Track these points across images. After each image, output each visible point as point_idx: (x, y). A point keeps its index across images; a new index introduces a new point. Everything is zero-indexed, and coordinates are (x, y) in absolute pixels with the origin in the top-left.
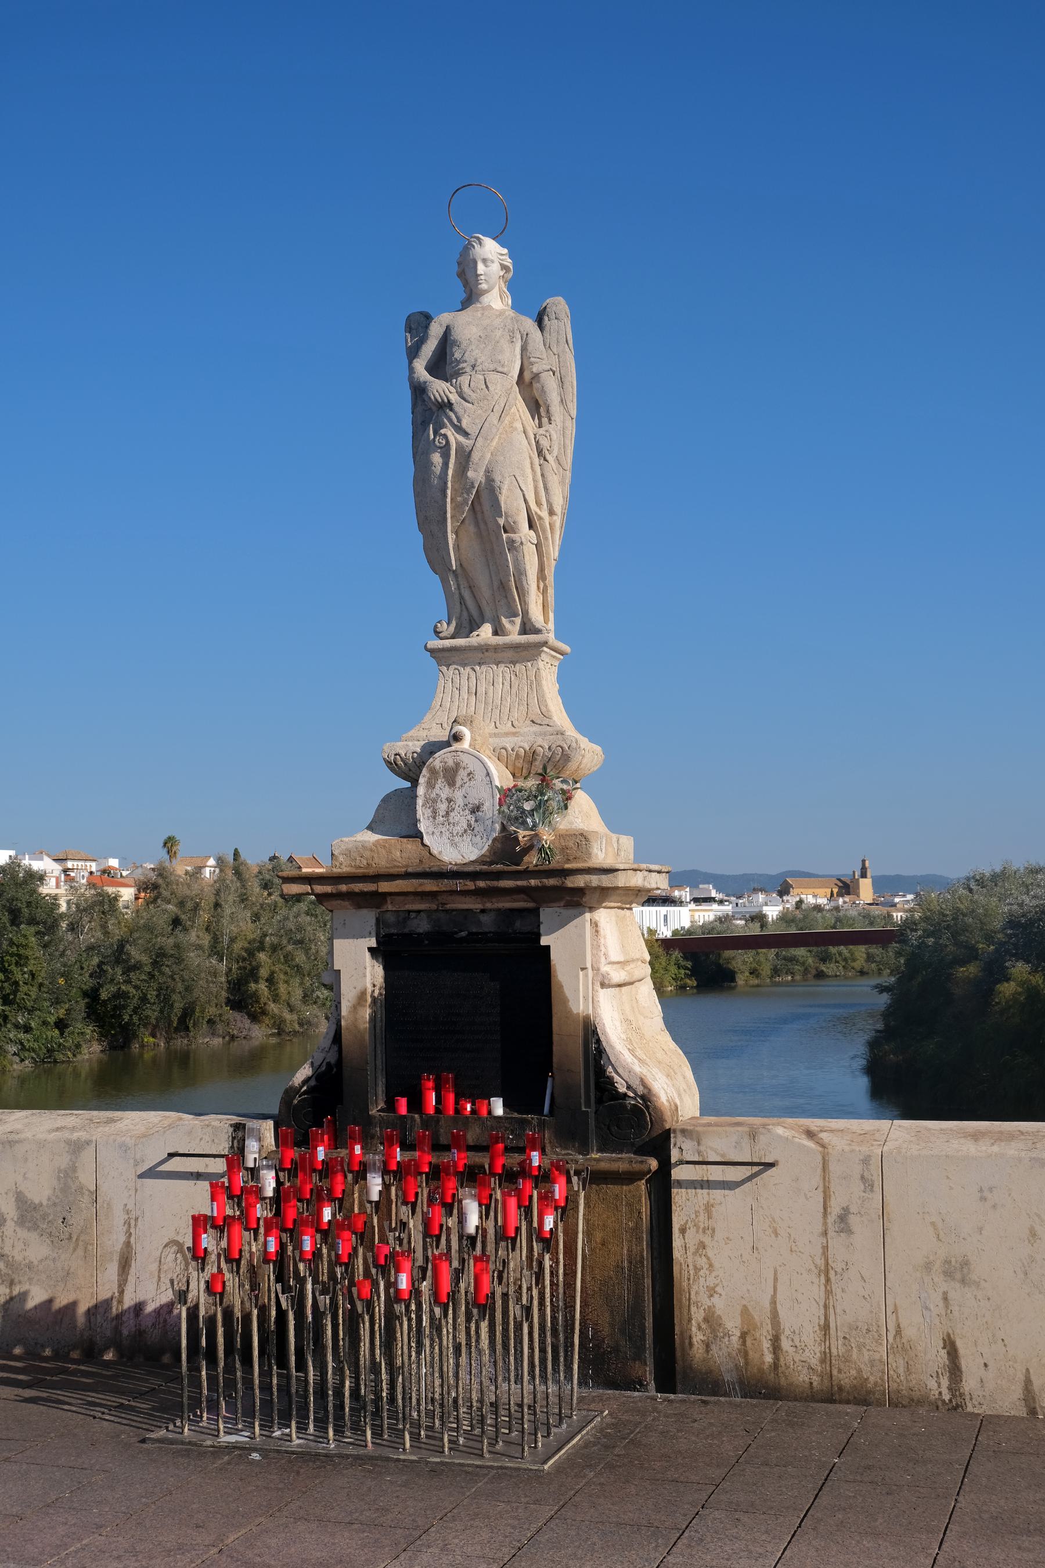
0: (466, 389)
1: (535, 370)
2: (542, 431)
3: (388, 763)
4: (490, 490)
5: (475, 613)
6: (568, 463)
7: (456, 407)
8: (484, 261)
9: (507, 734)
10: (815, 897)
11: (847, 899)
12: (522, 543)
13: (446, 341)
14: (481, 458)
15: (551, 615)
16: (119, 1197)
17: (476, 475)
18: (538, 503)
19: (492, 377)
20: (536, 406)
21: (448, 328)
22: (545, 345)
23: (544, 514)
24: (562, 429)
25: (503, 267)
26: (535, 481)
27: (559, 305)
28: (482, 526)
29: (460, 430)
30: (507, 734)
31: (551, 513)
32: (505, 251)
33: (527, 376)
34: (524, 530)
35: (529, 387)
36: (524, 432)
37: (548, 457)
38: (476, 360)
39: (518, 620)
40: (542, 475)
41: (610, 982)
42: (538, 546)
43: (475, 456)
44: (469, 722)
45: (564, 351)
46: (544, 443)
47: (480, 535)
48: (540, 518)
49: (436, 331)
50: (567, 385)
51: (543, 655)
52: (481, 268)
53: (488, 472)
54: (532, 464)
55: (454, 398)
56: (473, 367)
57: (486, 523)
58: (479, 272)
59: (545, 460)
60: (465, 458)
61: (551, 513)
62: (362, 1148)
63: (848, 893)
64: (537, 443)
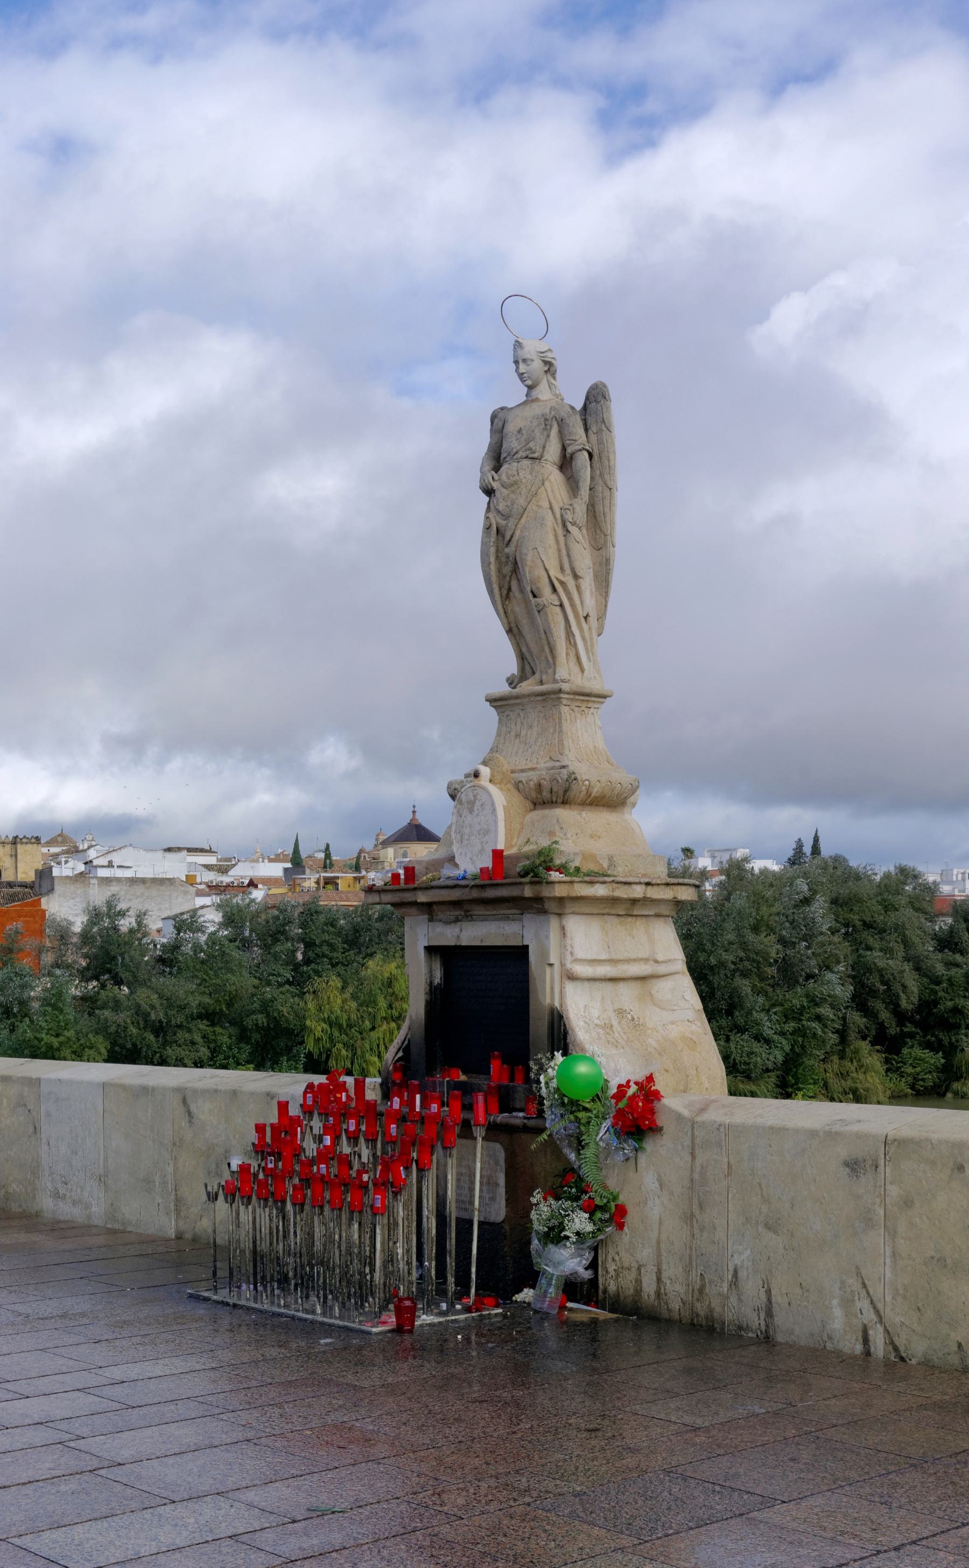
18: (562, 569)
26: (559, 550)
64: (562, 516)
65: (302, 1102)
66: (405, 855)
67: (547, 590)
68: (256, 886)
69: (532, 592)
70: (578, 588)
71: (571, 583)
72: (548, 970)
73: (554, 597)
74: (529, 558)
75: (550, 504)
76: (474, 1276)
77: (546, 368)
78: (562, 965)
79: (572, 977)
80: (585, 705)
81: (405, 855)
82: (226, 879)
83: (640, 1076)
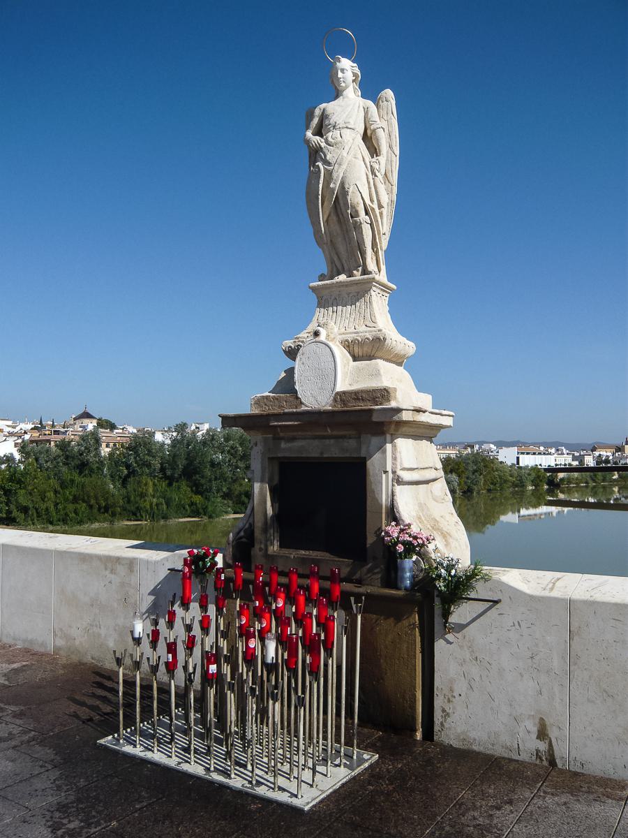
0: (330, 139)
1: (372, 128)
2: (373, 160)
3: (285, 351)
4: (343, 191)
5: (340, 268)
6: (394, 178)
7: (325, 150)
8: (343, 70)
9: (351, 333)
10: (606, 453)
11: (619, 453)
12: (361, 223)
13: (324, 116)
14: (338, 174)
15: (383, 267)
16: (77, 592)
17: (335, 185)
18: (372, 201)
19: (345, 132)
20: (374, 151)
21: (324, 110)
22: (379, 116)
23: (375, 206)
24: (390, 158)
25: (355, 75)
26: (370, 188)
27: (389, 93)
28: (341, 216)
29: (327, 163)
30: (351, 333)
31: (380, 206)
32: (355, 65)
33: (369, 132)
34: (362, 216)
35: (369, 139)
36: (364, 161)
37: (377, 173)
38: (336, 123)
39: (360, 269)
40: (374, 184)
41: (416, 496)
42: (371, 225)
43: (335, 175)
44: (325, 325)
45: (391, 118)
46: (376, 166)
47: (339, 221)
48: (373, 209)
49: (317, 112)
50: (393, 137)
51: (374, 288)
52: (340, 75)
53: (342, 184)
54: (367, 178)
55: (323, 145)
56: (334, 127)
57: (343, 215)
58: (339, 76)
59: (376, 176)
60: (329, 176)
61: (380, 206)
62: (547, 489)
63: (620, 451)
64: (371, 166)
65: (181, 595)
66: (82, 423)
67: (362, 213)
68: (27, 433)
69: (374, 151)
70: (381, 214)
71: (377, 211)
72: (384, 476)
73: (367, 217)
74: (350, 191)
75: (363, 158)
76: (283, 423)
77: (354, 78)
78: (394, 472)
79: (399, 481)
80: (382, 293)
81: (82, 423)
82: (16, 430)
83: (424, 534)
